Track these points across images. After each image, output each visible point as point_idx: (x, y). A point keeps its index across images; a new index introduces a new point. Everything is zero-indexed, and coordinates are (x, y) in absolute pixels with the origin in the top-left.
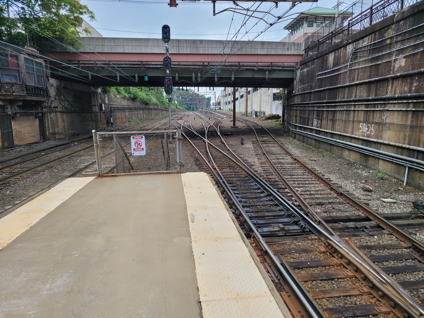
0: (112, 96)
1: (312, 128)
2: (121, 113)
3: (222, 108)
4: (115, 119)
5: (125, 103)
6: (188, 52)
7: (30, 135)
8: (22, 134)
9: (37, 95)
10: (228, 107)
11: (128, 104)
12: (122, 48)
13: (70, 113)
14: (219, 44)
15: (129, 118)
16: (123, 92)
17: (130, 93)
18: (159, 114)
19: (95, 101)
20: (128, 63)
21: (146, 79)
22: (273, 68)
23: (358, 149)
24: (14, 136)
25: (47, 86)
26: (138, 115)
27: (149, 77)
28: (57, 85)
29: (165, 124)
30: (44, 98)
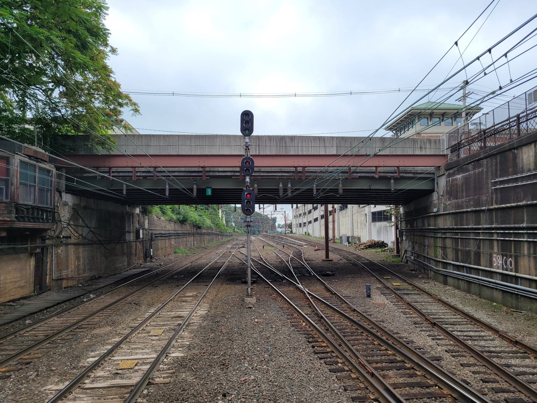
0: (154, 219)
1: (492, 270)
3: (294, 231)
5: (171, 227)
6: (273, 153)
7: (17, 285)
9: (35, 219)
13: (88, 244)
16: (169, 212)
17: (179, 213)
20: (183, 169)
21: (209, 192)
23: (516, 290)
25: (54, 205)
26: (187, 242)
29: (224, 255)
30: (47, 224)
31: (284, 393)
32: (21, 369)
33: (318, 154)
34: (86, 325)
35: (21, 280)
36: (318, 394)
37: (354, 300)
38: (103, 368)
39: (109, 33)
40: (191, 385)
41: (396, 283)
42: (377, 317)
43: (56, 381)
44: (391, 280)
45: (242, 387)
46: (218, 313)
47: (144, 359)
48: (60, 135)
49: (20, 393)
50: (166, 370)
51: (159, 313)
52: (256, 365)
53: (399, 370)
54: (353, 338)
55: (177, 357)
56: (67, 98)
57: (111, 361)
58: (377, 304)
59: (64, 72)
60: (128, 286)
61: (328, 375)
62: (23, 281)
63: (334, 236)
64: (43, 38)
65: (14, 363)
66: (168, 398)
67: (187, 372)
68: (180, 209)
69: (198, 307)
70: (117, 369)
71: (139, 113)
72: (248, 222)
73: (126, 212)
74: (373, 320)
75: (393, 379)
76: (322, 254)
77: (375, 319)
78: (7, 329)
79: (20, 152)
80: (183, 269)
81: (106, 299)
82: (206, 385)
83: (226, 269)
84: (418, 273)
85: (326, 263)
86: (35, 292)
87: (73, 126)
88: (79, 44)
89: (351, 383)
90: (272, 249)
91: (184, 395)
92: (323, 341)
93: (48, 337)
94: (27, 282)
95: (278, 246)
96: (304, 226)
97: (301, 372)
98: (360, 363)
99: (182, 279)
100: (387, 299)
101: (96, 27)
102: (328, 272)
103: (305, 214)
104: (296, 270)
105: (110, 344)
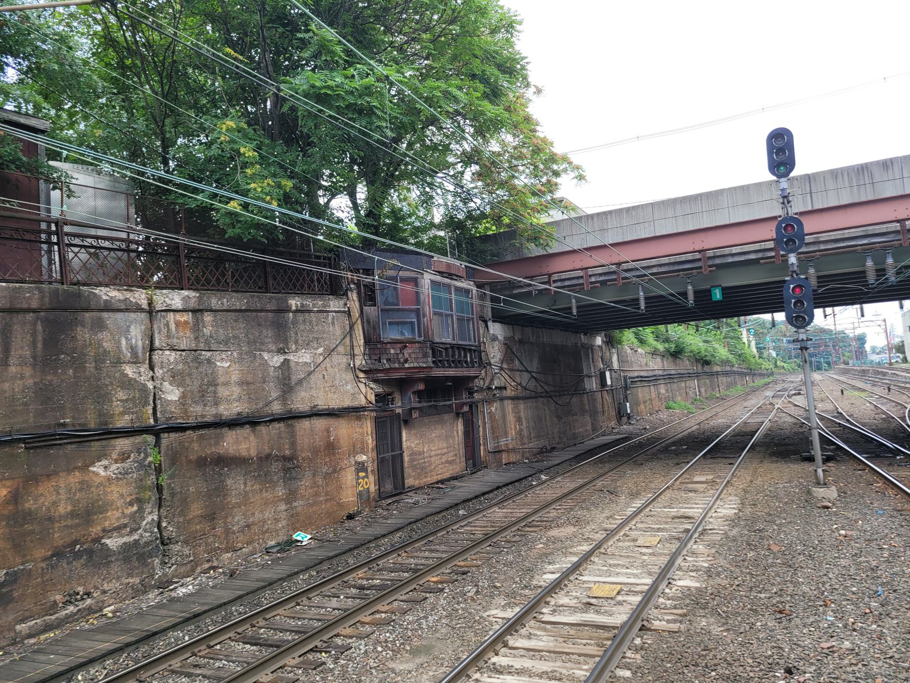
2: (648, 388)
4: (637, 403)
5: (656, 365)
7: (443, 460)
8: (424, 458)
9: (458, 363)
11: (664, 367)
15: (668, 399)
16: (651, 339)
17: (667, 340)
18: (736, 383)
20: (665, 260)
21: (717, 295)
24: (406, 465)
25: (479, 340)
26: (688, 390)
27: (724, 290)
28: (505, 338)
30: (472, 369)
32: (457, 580)
35: (448, 453)
38: (568, 592)
39: (527, 63)
40: (719, 641)
45: (825, 661)
46: (759, 514)
47: (631, 584)
48: (477, 238)
49: (456, 616)
50: (670, 609)
52: (852, 620)
55: (689, 589)
56: (482, 181)
57: (578, 582)
59: (475, 142)
60: (595, 462)
62: (452, 454)
64: (439, 94)
65: (448, 571)
66: (679, 659)
67: (708, 616)
68: (670, 333)
69: (718, 502)
70: (589, 597)
72: (803, 340)
73: (582, 344)
78: (437, 521)
79: (430, 268)
81: (566, 484)
82: (748, 645)
83: (766, 436)
87: (493, 219)
88: (487, 90)
90: (863, 395)
91: (708, 658)
93: (487, 537)
94: (456, 455)
95: (875, 388)
105: (575, 554)
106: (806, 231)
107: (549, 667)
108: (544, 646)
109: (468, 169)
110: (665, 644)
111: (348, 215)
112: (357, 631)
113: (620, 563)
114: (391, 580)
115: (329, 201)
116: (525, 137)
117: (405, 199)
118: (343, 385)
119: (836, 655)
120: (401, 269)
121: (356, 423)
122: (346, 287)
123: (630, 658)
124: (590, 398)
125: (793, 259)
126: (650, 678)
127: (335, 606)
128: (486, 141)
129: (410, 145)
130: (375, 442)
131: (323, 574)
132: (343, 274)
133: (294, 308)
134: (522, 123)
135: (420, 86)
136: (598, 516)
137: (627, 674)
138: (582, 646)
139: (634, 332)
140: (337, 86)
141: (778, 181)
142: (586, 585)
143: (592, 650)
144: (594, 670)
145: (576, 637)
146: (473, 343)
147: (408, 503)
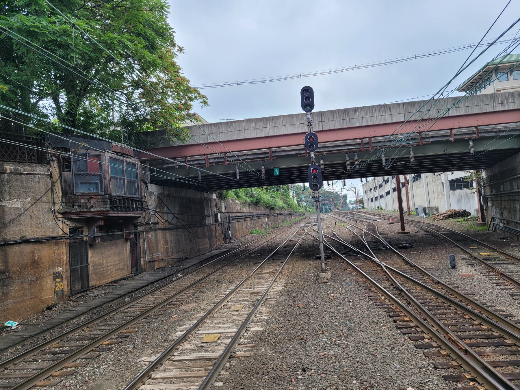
3: (366, 206)
5: (246, 210)
7: (117, 268)
8: (103, 268)
9: (127, 209)
10: (375, 205)
11: (250, 210)
12: (242, 133)
13: (174, 229)
14: (383, 109)
16: (243, 195)
17: (252, 196)
18: (286, 220)
19: (208, 210)
21: (277, 172)
22: (480, 135)
24: (90, 272)
30: (137, 212)
31: (367, 369)
32: (121, 342)
33: (384, 122)
34: (175, 301)
35: (120, 263)
36: (404, 371)
37: (437, 272)
38: (190, 341)
39: (173, 32)
40: (270, 359)
41: (484, 254)
42: (465, 290)
43: (150, 353)
44: (478, 250)
45: (321, 362)
47: (226, 333)
48: (141, 133)
49: (119, 364)
50: (246, 344)
51: (238, 290)
52: (334, 339)
53: (497, 346)
54: (439, 312)
55: (257, 332)
57: (196, 334)
58: (465, 275)
59: (141, 75)
60: (211, 265)
61: (414, 351)
63: (409, 209)
64: (115, 42)
65: (115, 337)
66: (249, 372)
67: (266, 346)
68: (253, 192)
69: (275, 283)
70: (202, 343)
71: (208, 105)
73: (205, 198)
74: (461, 292)
75: (492, 357)
76: (397, 227)
77: (463, 292)
78: (110, 306)
79: (109, 149)
80: (259, 248)
81: (193, 278)
82: (285, 359)
83: (300, 247)
84: (509, 241)
85: (402, 236)
86: (132, 273)
87: (151, 122)
89: (442, 360)
90: (345, 225)
91: (264, 369)
92: (405, 316)
93: (143, 313)
94: (125, 265)
95: (350, 221)
96: (376, 200)
97: (383, 347)
98: (450, 339)
99: (259, 257)
100: (476, 270)
101: (162, 28)
102: (405, 245)
103: (376, 188)
104: (371, 244)
105: (195, 319)
106: (319, 141)
107: (175, 387)
108: (174, 375)
109: (136, 91)
110: (242, 364)
111: (51, 112)
112: (50, 382)
113: (221, 321)
114: (76, 346)
115: (38, 101)
116: (172, 75)
117: (94, 106)
118: (45, 222)
119: (327, 358)
120: (89, 149)
121: (54, 247)
122: (49, 158)
123: (222, 375)
124: (209, 229)
125: (313, 155)
126: (233, 384)
127: (34, 367)
128: (148, 76)
129: (97, 72)
130: (68, 259)
131: (27, 347)
132: (47, 150)
133: (8, 171)
134: (170, 67)
135: (103, 35)
136: (210, 295)
137: (221, 384)
138: (196, 372)
139: (234, 192)
140: (42, 27)
141: (306, 114)
142: (201, 336)
143: (202, 373)
144: (202, 385)
145: (193, 367)
146: (137, 196)
147: (91, 296)
